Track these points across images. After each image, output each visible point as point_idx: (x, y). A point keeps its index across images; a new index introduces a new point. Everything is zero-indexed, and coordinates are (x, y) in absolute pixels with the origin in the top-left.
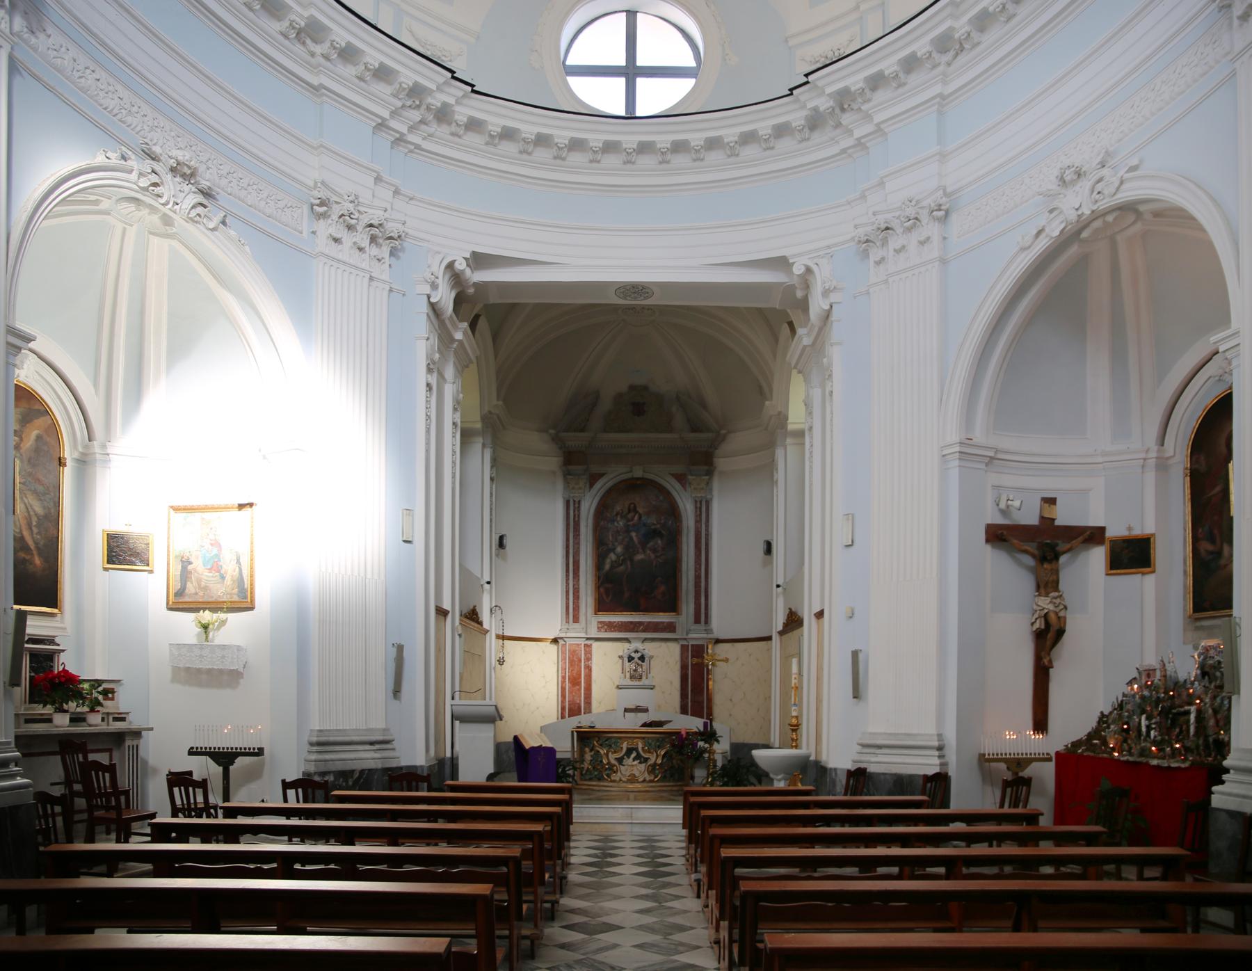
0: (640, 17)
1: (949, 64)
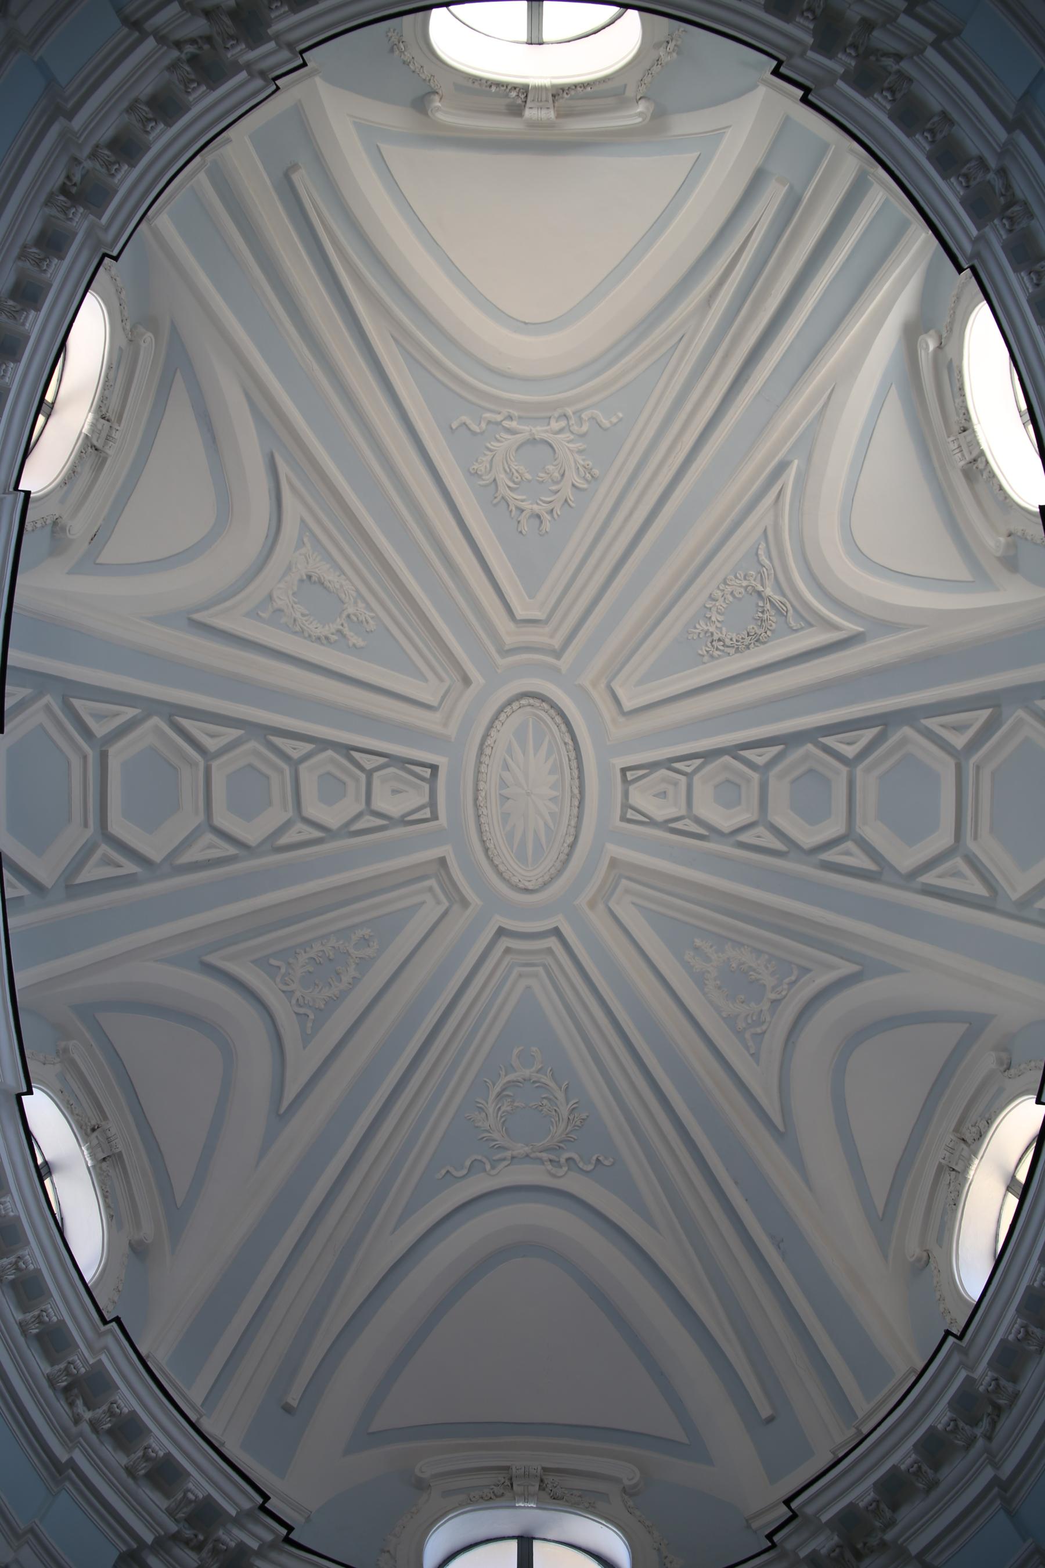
0: (537, 1546)
1: (989, 1438)
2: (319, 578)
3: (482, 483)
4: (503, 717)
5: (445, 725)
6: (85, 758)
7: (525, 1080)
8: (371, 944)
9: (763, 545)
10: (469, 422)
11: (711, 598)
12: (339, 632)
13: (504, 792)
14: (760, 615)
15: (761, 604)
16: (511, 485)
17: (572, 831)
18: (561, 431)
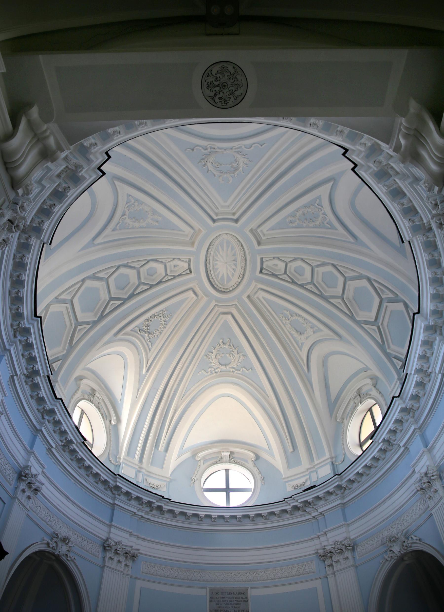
2: (297, 333)
3: (242, 353)
4: (236, 286)
5: (256, 285)
6: (382, 324)
7: (226, 173)
8: (289, 221)
9: (150, 347)
10: (246, 371)
11: (164, 328)
12: (292, 316)
13: (234, 262)
14: (148, 327)
15: (148, 330)
16: (233, 353)
17: (209, 253)
18: (217, 368)
